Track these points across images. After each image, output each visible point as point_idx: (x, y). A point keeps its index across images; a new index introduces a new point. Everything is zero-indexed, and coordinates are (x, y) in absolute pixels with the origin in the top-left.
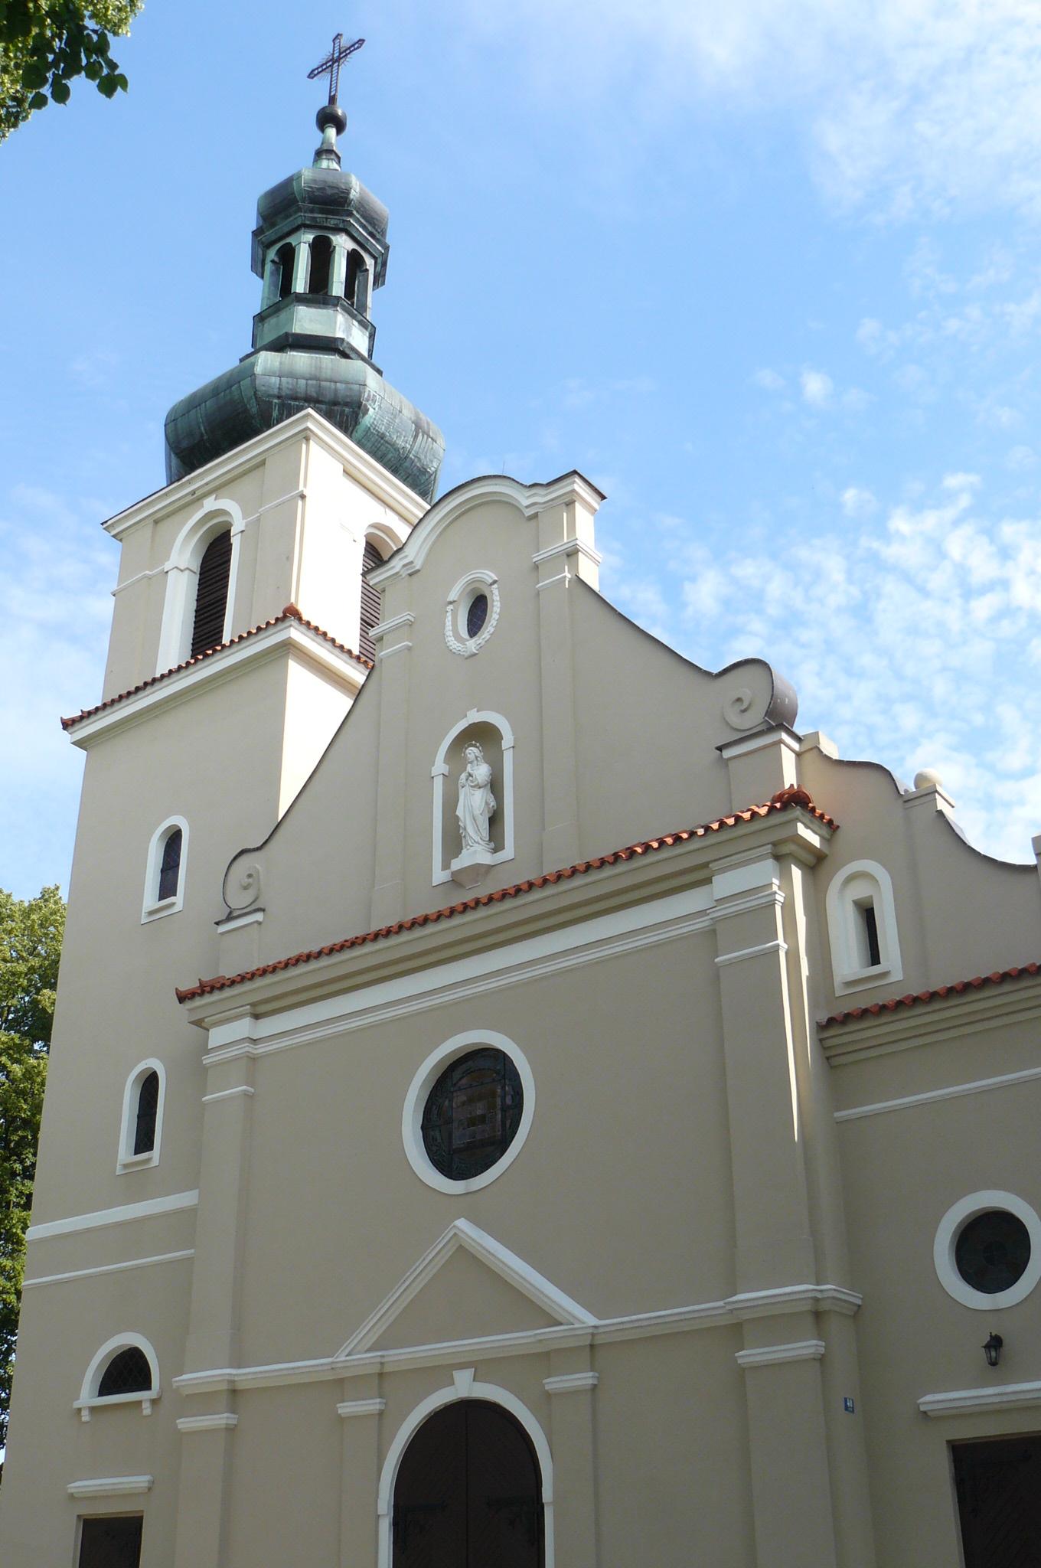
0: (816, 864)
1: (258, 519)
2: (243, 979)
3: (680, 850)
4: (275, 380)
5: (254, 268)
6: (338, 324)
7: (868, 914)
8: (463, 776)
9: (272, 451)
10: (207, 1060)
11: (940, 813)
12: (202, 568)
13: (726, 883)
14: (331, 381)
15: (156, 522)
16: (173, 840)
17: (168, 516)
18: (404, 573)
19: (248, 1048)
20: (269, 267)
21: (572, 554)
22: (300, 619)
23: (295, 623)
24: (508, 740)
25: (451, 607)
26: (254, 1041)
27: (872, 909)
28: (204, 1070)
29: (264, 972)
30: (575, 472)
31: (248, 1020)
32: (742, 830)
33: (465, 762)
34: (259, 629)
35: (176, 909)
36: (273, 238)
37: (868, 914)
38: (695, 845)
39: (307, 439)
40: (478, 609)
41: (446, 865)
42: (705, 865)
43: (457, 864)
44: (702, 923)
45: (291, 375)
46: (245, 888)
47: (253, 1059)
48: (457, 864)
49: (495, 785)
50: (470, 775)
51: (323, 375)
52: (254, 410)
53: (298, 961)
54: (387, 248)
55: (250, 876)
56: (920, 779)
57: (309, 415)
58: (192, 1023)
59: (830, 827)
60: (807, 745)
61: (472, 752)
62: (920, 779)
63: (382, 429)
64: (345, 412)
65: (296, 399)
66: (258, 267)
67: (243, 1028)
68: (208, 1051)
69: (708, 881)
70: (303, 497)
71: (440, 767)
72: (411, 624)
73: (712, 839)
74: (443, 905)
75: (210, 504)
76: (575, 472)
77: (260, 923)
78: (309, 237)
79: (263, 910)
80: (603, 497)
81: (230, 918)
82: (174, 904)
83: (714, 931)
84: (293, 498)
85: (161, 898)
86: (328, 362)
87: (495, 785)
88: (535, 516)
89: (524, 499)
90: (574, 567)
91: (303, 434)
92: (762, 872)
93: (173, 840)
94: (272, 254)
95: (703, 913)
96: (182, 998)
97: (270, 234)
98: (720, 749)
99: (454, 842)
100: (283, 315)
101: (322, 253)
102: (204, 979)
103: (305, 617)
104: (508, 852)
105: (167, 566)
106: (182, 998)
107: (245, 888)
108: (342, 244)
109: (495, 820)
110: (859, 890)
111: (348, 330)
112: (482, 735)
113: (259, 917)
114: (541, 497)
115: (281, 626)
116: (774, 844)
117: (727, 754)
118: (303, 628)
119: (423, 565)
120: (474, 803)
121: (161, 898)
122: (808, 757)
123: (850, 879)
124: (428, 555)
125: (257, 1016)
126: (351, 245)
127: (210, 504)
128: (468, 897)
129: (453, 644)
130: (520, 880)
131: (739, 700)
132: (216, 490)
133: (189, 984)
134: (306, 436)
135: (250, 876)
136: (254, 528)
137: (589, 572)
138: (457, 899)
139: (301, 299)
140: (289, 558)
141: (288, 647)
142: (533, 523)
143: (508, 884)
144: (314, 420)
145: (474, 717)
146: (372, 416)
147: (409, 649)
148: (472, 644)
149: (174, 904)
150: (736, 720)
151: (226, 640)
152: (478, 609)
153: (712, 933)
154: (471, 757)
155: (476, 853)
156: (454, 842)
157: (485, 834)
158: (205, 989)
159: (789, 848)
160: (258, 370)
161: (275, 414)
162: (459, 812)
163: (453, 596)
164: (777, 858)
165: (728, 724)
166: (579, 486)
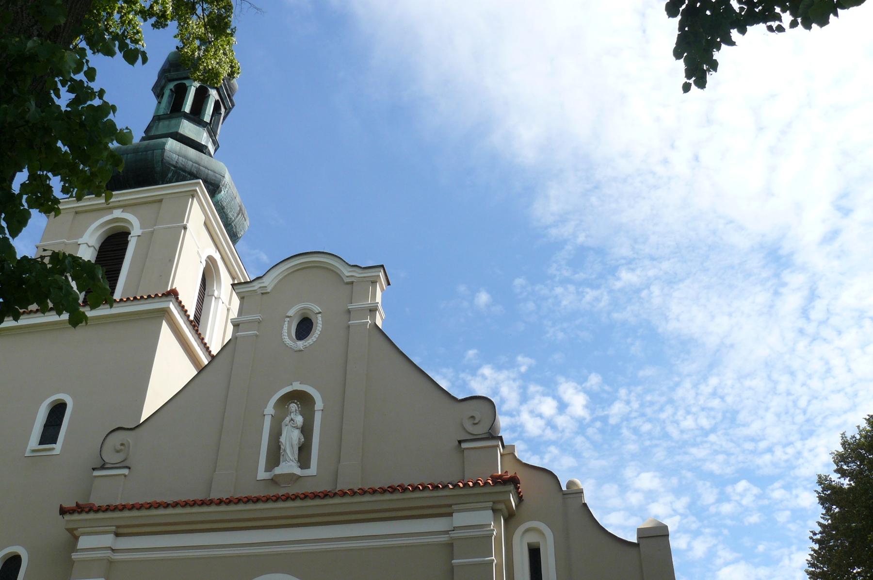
0: (510, 518)
1: (152, 232)
2: (108, 509)
3: (435, 494)
4: (175, 156)
5: (154, 89)
6: (203, 138)
7: (535, 554)
8: (288, 419)
9: (168, 196)
10: (74, 556)
11: (585, 505)
12: (101, 247)
13: (461, 519)
14: (206, 168)
15: (76, 213)
16: (57, 411)
17: (86, 212)
18: (259, 292)
19: (108, 553)
20: (167, 93)
21: (373, 310)
22: (177, 298)
23: (174, 300)
24: (319, 405)
25: (288, 319)
26: (113, 550)
27: (539, 549)
28: (72, 563)
29: (132, 507)
30: (382, 266)
31: (112, 536)
32: (477, 490)
33: (288, 413)
34: (149, 297)
35: (54, 453)
36: (175, 77)
37: (535, 554)
38: (445, 493)
39: (193, 196)
40: (304, 327)
41: (269, 469)
42: (450, 506)
43: (278, 471)
44: (444, 538)
45: (185, 157)
46: (118, 452)
47: (111, 562)
48: (278, 471)
49: (306, 430)
50: (292, 420)
51: (202, 163)
52: (158, 169)
53: (150, 506)
54: (233, 105)
55: (122, 445)
56: (570, 484)
57: (199, 183)
58: (67, 530)
59: (520, 499)
60: (506, 452)
61: (293, 407)
62: (570, 484)
63: (225, 204)
64: (214, 188)
65: (184, 171)
66: (158, 91)
67: (108, 540)
68: (77, 551)
69: (450, 515)
70: (185, 228)
71: (270, 410)
72: (259, 322)
73: (457, 492)
74: (262, 494)
75: (118, 213)
76: (382, 266)
77: (125, 476)
78: (197, 84)
79: (129, 468)
80: (389, 284)
81: (103, 467)
82: (53, 449)
83: (452, 544)
84: (179, 227)
85: (41, 443)
86: (192, 152)
87: (306, 430)
88: (352, 283)
89: (346, 272)
90: (374, 318)
91: (191, 193)
92: (485, 517)
93: (57, 411)
94: (172, 86)
95: (447, 532)
96: (63, 511)
97: (173, 74)
98: (460, 442)
99: (275, 456)
100: (173, 122)
101: (201, 96)
102: (80, 503)
103: (180, 298)
104: (313, 470)
105: (80, 241)
106: (63, 511)
107: (118, 452)
108: (214, 94)
109: (304, 450)
110: (532, 538)
111: (207, 142)
112: (302, 399)
113: (126, 471)
114: (358, 274)
115: (164, 299)
116: (494, 502)
117: (464, 445)
118: (176, 304)
119: (272, 290)
120: (291, 437)
121: (41, 443)
122: (507, 458)
123: (527, 530)
124: (275, 286)
125: (117, 535)
126: (217, 98)
127: (118, 213)
128: (282, 492)
129: (287, 341)
130: (318, 489)
131: (473, 417)
132: (124, 207)
133: (70, 504)
134: (193, 194)
135: (122, 445)
136: (147, 239)
137: (379, 323)
138: (273, 491)
139: (186, 116)
140: (171, 261)
141: (165, 313)
142: (349, 286)
143: (309, 490)
144: (201, 189)
145: (297, 386)
146: (223, 194)
147: (257, 336)
148: (301, 344)
149: (53, 449)
150: (470, 428)
151: (117, 296)
152: (304, 327)
153: (450, 546)
154: (293, 409)
155: (289, 466)
156: (275, 456)
157: (296, 457)
158: (79, 509)
159: (502, 506)
160: (167, 147)
161: (170, 175)
162: (283, 439)
163: (291, 313)
164: (495, 511)
165: (464, 429)
166: (382, 275)
